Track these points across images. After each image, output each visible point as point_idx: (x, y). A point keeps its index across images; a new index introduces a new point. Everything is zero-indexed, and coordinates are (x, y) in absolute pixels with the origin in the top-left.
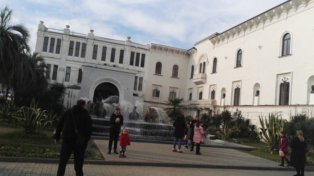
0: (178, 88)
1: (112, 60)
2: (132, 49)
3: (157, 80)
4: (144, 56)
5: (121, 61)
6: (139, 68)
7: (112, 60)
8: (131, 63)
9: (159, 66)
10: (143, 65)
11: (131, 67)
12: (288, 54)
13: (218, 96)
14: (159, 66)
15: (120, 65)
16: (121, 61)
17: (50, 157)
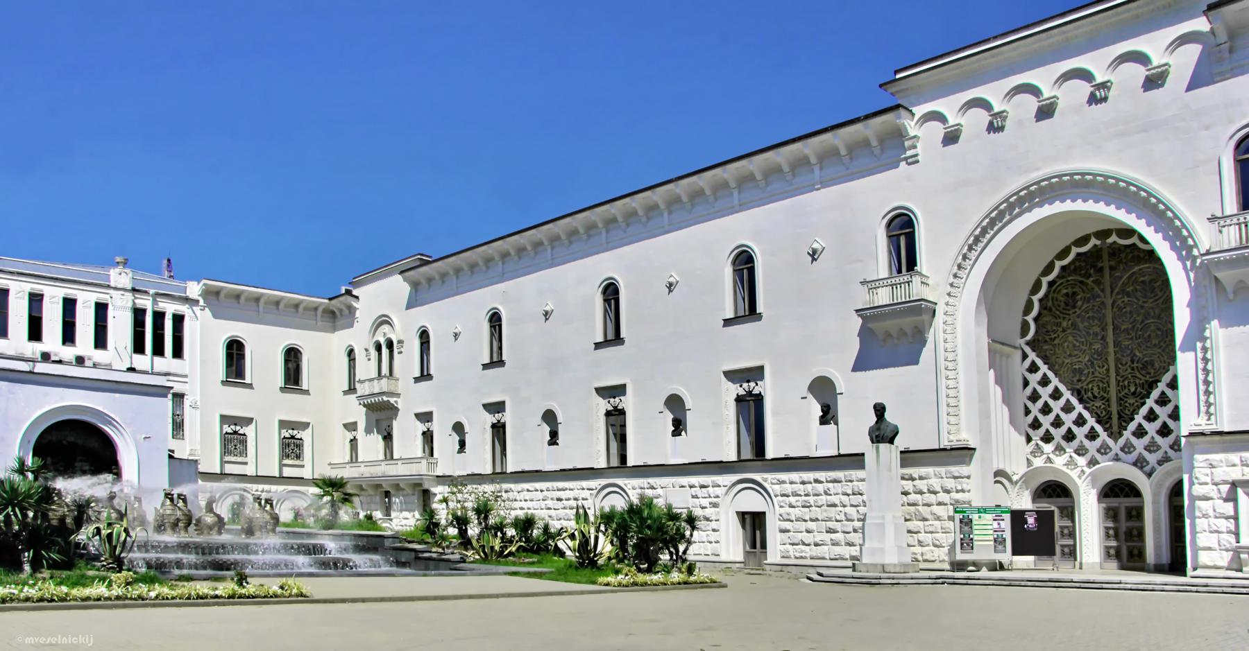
0: (308, 424)
1: (69, 336)
2: (285, 469)
3: (235, 401)
4: (178, 320)
5: (100, 341)
6: (166, 362)
7: (69, 336)
8: (139, 348)
9: (235, 351)
10: (178, 352)
11: (142, 362)
12: (555, 443)
13: (445, 441)
14: (235, 351)
15: (99, 356)
16: (100, 341)
17: (131, 599)
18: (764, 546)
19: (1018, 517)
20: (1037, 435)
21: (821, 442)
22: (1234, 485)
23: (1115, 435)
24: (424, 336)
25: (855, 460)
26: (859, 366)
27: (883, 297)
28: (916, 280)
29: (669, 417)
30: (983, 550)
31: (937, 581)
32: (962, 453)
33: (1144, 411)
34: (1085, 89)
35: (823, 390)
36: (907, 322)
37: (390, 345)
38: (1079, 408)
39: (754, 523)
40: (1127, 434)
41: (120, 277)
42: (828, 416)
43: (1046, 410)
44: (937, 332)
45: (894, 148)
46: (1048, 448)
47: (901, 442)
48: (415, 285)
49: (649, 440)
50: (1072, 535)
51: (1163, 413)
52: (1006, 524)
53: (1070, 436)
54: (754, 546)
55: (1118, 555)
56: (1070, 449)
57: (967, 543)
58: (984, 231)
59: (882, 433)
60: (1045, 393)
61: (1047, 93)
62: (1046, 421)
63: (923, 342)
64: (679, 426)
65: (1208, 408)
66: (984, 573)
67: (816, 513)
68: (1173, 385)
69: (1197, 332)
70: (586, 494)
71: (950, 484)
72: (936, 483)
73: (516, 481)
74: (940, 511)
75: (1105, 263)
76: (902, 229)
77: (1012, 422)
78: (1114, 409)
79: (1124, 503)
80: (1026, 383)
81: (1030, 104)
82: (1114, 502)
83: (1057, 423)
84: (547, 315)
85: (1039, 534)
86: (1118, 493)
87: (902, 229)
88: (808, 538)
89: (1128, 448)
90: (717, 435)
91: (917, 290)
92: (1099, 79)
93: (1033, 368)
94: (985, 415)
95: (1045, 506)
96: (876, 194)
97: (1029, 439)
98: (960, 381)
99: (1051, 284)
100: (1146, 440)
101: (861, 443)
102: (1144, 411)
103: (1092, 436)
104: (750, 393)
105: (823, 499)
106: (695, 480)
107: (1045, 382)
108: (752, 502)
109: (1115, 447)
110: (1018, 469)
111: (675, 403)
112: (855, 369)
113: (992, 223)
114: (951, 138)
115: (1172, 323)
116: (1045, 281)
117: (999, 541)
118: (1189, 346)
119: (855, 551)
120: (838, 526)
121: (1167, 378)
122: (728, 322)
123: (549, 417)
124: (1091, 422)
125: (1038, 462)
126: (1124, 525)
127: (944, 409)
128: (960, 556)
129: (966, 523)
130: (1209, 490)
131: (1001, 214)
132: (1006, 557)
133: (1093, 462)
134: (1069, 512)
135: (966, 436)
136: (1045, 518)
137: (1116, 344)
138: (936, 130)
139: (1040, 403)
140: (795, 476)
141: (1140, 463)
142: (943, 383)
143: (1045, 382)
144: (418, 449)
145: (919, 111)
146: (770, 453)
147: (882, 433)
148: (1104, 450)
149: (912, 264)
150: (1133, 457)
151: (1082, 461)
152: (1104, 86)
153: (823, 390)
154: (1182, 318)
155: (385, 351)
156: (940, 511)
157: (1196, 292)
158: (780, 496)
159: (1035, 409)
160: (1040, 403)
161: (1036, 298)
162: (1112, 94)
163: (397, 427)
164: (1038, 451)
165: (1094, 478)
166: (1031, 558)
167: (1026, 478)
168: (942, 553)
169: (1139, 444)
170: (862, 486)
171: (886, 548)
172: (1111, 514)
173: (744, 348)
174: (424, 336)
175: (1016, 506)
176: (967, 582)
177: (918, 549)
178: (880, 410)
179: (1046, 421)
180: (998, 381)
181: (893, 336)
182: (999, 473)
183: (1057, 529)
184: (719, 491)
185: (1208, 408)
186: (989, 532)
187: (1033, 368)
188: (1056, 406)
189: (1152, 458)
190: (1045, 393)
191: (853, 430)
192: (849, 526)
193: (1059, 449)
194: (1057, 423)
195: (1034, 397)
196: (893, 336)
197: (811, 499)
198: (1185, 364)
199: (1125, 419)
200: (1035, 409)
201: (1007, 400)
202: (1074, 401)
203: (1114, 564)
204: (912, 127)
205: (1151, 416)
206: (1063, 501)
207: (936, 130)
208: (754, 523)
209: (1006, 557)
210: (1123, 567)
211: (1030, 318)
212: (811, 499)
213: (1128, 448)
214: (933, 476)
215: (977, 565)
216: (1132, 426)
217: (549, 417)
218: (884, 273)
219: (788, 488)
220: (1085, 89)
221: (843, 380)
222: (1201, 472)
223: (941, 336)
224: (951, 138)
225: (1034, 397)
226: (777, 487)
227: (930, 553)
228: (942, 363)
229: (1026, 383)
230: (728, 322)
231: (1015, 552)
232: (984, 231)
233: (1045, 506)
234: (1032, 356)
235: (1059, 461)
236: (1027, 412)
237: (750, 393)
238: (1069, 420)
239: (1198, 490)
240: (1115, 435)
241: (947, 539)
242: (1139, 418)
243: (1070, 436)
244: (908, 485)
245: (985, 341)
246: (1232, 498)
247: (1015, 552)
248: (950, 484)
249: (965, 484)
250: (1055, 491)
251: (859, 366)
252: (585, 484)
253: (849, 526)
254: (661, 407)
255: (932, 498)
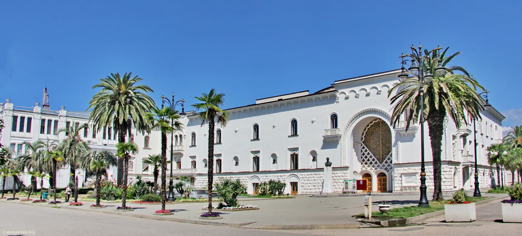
18: (297, 190)
19: (358, 182)
20: (364, 163)
21: (313, 165)
22: (402, 174)
23: (381, 163)
24: (194, 135)
25: (322, 170)
26: (323, 148)
27: (329, 134)
28: (337, 130)
29: (272, 159)
30: (350, 189)
31: (340, 196)
32: (346, 168)
33: (387, 158)
34: (376, 91)
35: (314, 154)
36: (335, 139)
37: (181, 136)
38: (373, 157)
39: (294, 185)
40: (384, 163)
41: (63, 112)
42: (314, 159)
43: (366, 157)
44: (341, 141)
45: (333, 99)
46: (366, 166)
47: (332, 166)
48: (191, 120)
49: (265, 164)
50: (371, 185)
51: (389, 161)
52: (356, 183)
53: (371, 163)
54: (294, 190)
55: (381, 190)
56: (371, 166)
57: (347, 188)
58: (353, 119)
59: (328, 164)
60: (366, 153)
61: (368, 91)
62: (366, 160)
63: (338, 143)
64: (275, 161)
65: (397, 159)
66: (350, 194)
67: (311, 182)
68: (391, 156)
69: (396, 143)
70: (247, 178)
71: (343, 175)
72: (340, 175)
73: (225, 175)
74: (341, 181)
75: (380, 125)
76: (334, 118)
77: (358, 160)
78: (381, 157)
79: (382, 178)
80: (362, 151)
81: (364, 93)
82: (380, 178)
83: (368, 160)
84: (236, 131)
85: (362, 186)
86: (381, 175)
87: (334, 118)
88: (308, 188)
89: (384, 166)
90: (285, 163)
91: (337, 132)
92: (379, 90)
93: (364, 148)
94: (352, 159)
95: (365, 179)
96: (328, 110)
97: (362, 164)
98: (347, 153)
99: (368, 129)
100: (388, 164)
101: (323, 166)
102: (387, 158)
103: (376, 163)
104: (294, 154)
105: (313, 179)
106: (279, 174)
107: (366, 151)
108: (294, 180)
109: (381, 165)
110: (359, 171)
111: (274, 156)
112: (322, 149)
113: (355, 118)
114: (347, 98)
115: (391, 140)
116: (370, 125)
117: (354, 187)
118: (395, 146)
119: (321, 190)
120: (316, 185)
121: (390, 154)
122: (289, 137)
123: (236, 158)
124: (376, 160)
125: (364, 169)
126: (382, 183)
127: (342, 158)
128: (345, 191)
129: (347, 183)
130: (397, 175)
131: (357, 116)
132: (355, 190)
133: (376, 169)
134: (371, 180)
135: (347, 164)
136: (365, 182)
137: (382, 143)
138: (344, 96)
139: (365, 156)
140: (306, 173)
141: (386, 169)
142: (342, 153)
143: (366, 151)
144: (190, 166)
145: (340, 91)
146: (299, 168)
147: (328, 164)
148: (378, 166)
149: (336, 127)
150: (385, 168)
151: (373, 169)
152: (380, 91)
153: (314, 154)
154: (393, 140)
155: (179, 138)
156: (341, 181)
157: (396, 135)
158: (301, 179)
159: (364, 157)
160: (365, 156)
161: (365, 132)
162: (382, 93)
163: (182, 160)
164: (364, 166)
165: (376, 172)
166: (361, 191)
167: (361, 173)
168: (341, 190)
169: (386, 165)
170: (322, 176)
171: (328, 189)
172: (379, 180)
173: (294, 142)
174: (194, 135)
175: (358, 179)
176: (346, 196)
177: (335, 189)
178: (328, 159)
179: (366, 160)
180: (355, 151)
181: (331, 142)
182: (354, 172)
183: (367, 184)
184: (285, 177)
185: (397, 159)
186: (352, 185)
187: (364, 148)
188: (368, 156)
189: (389, 168)
190: (366, 153)
191: (321, 163)
192: (319, 185)
193: (369, 166)
194: (368, 160)
195: (363, 154)
196: (331, 142)
197: (310, 179)
198: (394, 149)
199: (383, 159)
200: (364, 157)
201: (357, 155)
202: (372, 155)
203: (380, 191)
204: (338, 95)
205: (386, 162)
206: (369, 178)
207: (344, 96)
208: (294, 185)
209: (355, 190)
210: (382, 192)
211: (363, 137)
212: (310, 179)
213: (384, 166)
214: (339, 173)
215: (349, 192)
216: (385, 161)
217: (236, 158)
218: (329, 128)
219: (304, 176)
220: (376, 91)
221: (319, 151)
222: (396, 171)
223: (342, 142)
224: (347, 98)
225: (363, 154)
226: (301, 176)
227: (338, 190)
228: (342, 148)
229: (362, 151)
230: (289, 137)
231: (358, 189)
232: (353, 119)
233: (365, 179)
234: (363, 145)
235: (369, 169)
236: (362, 158)
237: (294, 154)
238: (371, 159)
239: (395, 175)
240: (381, 163)
241: (342, 187)
242: (386, 159)
243: (371, 163)
244: (333, 175)
245: (352, 142)
246: (401, 177)
247: (358, 189)
248: (343, 175)
249: (347, 175)
250: (368, 175)
251: (323, 148)
252: (246, 176)
253: (319, 185)
254: (270, 156)
255: (339, 178)
